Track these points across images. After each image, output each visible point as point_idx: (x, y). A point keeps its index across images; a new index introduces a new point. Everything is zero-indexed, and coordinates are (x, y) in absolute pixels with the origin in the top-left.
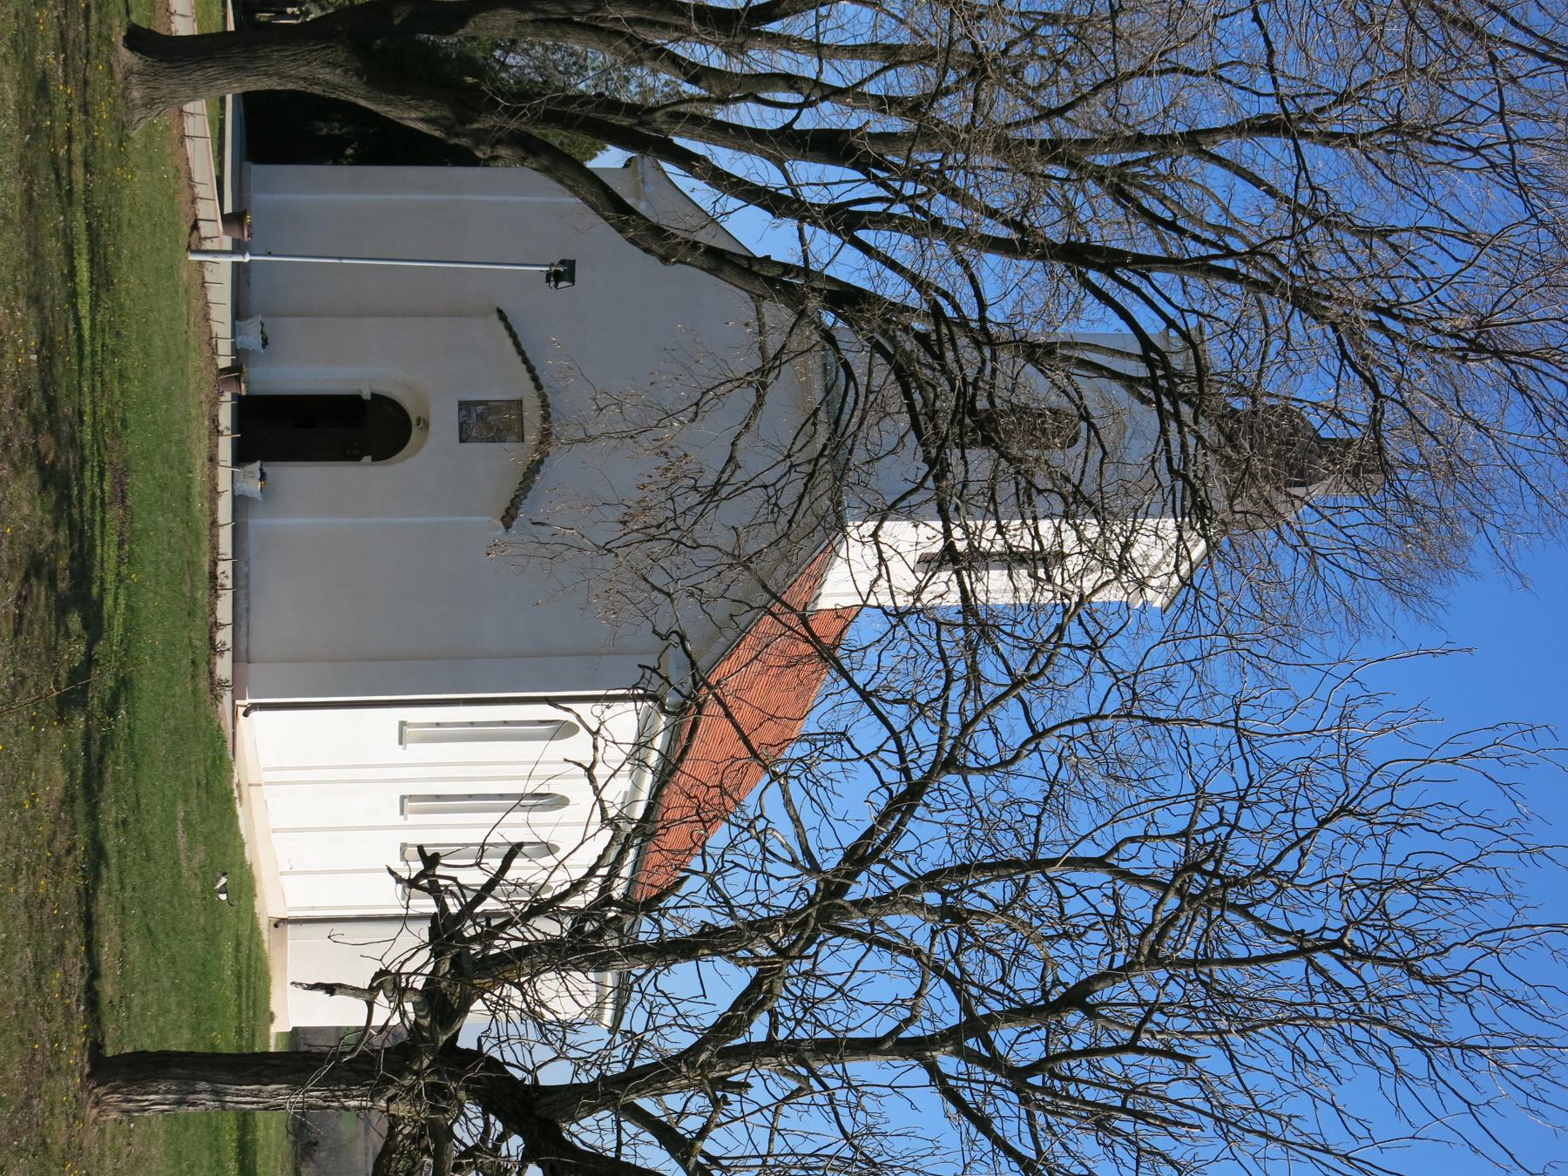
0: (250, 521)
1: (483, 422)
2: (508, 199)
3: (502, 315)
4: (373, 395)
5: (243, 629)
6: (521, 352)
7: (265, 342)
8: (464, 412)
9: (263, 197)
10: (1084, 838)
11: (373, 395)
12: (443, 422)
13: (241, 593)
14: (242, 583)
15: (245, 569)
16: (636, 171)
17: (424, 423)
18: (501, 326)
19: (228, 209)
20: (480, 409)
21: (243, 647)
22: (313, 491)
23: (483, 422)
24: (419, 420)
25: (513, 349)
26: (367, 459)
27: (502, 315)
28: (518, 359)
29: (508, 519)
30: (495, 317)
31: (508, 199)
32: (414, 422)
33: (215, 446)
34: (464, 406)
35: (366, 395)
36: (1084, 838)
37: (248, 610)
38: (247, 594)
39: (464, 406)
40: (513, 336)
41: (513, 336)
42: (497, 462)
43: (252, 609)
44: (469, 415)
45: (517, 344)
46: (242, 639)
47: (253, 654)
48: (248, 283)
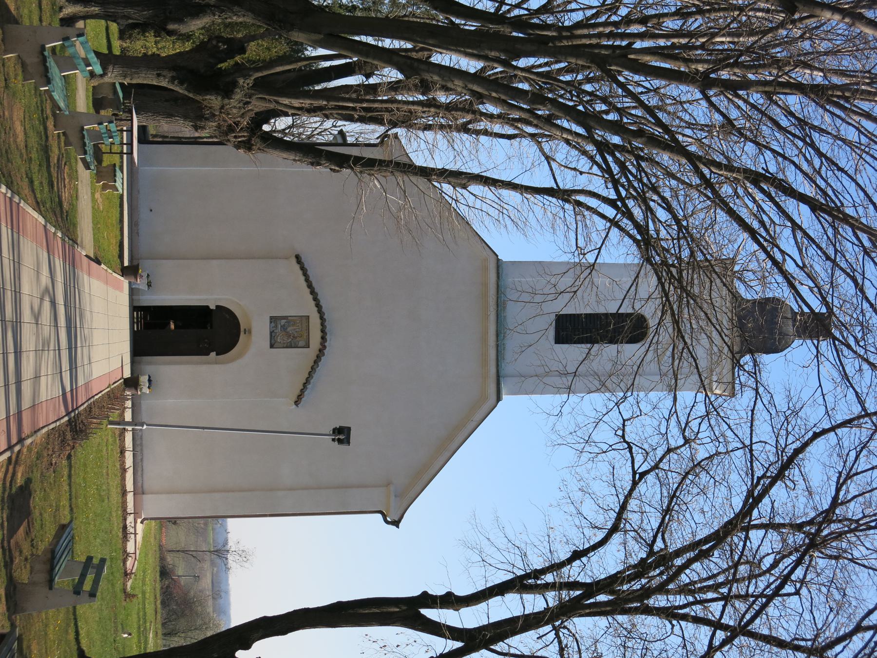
1: (286, 333)
3: (298, 258)
4: (217, 306)
5: (139, 473)
7: (149, 285)
8: (273, 324)
10: (624, 425)
11: (217, 306)
13: (138, 449)
14: (138, 442)
17: (248, 332)
18: (297, 267)
19: (126, 264)
21: (140, 484)
22: (180, 377)
23: (286, 333)
25: (304, 284)
26: (213, 354)
27: (298, 258)
28: (308, 291)
29: (297, 403)
32: (242, 329)
33: (123, 479)
34: (273, 319)
35: (213, 307)
36: (624, 425)
37: (142, 460)
38: (142, 450)
39: (273, 319)
42: (294, 360)
43: (145, 459)
44: (276, 326)
45: (307, 280)
46: (139, 479)
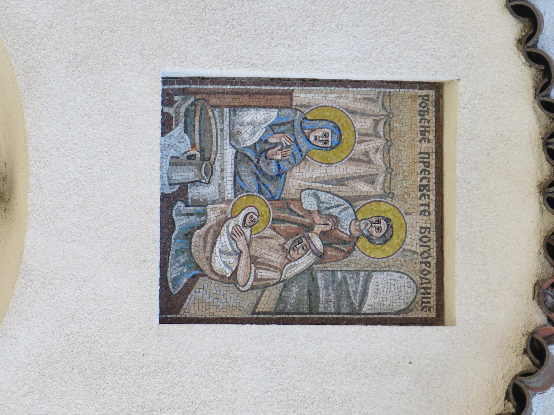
20: (255, 122)
34: (189, 101)
39: (189, 101)
44: (202, 159)
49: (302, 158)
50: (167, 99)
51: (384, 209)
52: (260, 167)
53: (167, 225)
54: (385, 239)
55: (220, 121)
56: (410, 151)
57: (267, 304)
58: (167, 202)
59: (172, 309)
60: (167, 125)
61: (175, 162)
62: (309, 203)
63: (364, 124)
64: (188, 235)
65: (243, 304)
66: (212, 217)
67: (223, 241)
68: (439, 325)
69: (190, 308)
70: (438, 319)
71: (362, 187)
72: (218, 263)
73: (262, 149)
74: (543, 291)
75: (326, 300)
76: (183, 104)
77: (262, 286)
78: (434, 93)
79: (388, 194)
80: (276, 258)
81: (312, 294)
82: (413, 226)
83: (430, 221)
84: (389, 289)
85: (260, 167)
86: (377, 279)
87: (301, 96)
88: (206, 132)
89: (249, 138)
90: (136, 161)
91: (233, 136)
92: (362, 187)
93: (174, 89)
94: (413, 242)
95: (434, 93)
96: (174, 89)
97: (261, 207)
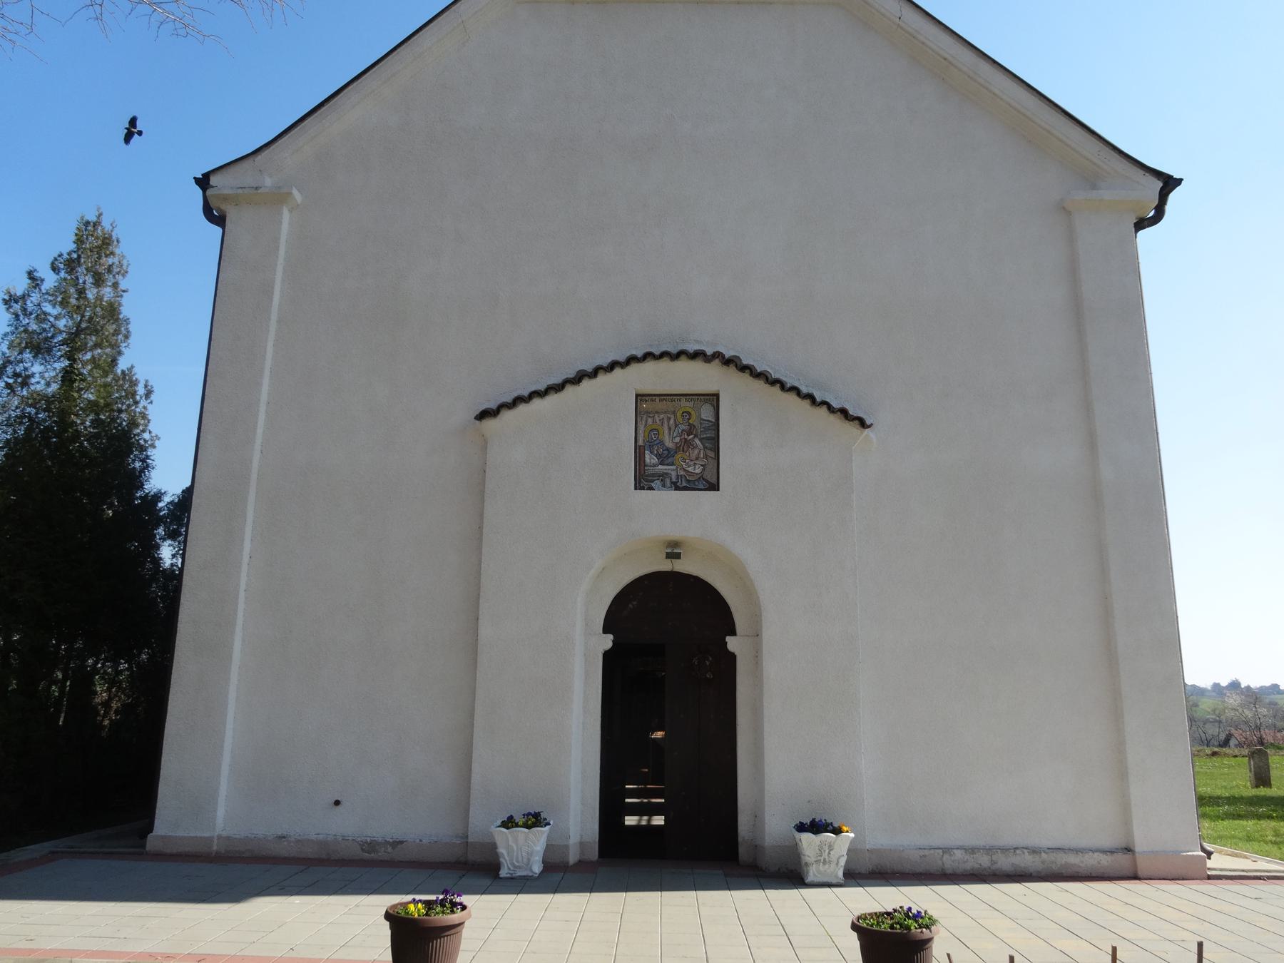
0: (215, 848)
1: (679, 447)
2: (264, 397)
3: (484, 415)
4: (606, 631)
5: (1073, 859)
6: (558, 388)
7: (535, 820)
9: (221, 812)
11: (606, 631)
12: (673, 515)
13: (1005, 863)
15: (958, 854)
16: (235, 200)
18: (506, 415)
20: (649, 458)
21: (1105, 861)
23: (679, 447)
24: (670, 556)
25: (552, 399)
26: (732, 643)
27: (484, 415)
28: (569, 390)
30: (490, 423)
31: (264, 397)
34: (643, 480)
35: (607, 642)
38: (1004, 850)
39: (643, 480)
40: (518, 400)
41: (518, 400)
42: (752, 434)
44: (662, 477)
47: (1108, 839)
48: (397, 844)
49: (662, 443)
50: (642, 488)
51: (679, 414)
52: (666, 456)
53: (685, 488)
54: (689, 414)
55: (650, 470)
56: (659, 405)
57: (712, 454)
58: (677, 488)
59: (714, 487)
60: (651, 488)
61: (664, 486)
62: (677, 440)
63: (650, 421)
64: (689, 481)
65: (712, 463)
66: (682, 473)
67: (690, 469)
68: (178, 590)
69: (714, 480)
70: (717, 396)
71: (672, 422)
72: (698, 471)
73: (659, 456)
74: (1248, 688)
75: (710, 434)
76: (644, 483)
77: (706, 456)
78: (640, 397)
79: (674, 413)
80: (696, 451)
81: (708, 439)
82: (686, 405)
83: (683, 398)
84: (706, 413)
85: (666, 456)
86: (703, 416)
87: (641, 442)
88: (653, 475)
89: (655, 460)
90: (664, 500)
91: (655, 466)
92: (672, 422)
93: (639, 486)
94: (691, 404)
95: (640, 397)
96: (639, 486)
97: (679, 456)
